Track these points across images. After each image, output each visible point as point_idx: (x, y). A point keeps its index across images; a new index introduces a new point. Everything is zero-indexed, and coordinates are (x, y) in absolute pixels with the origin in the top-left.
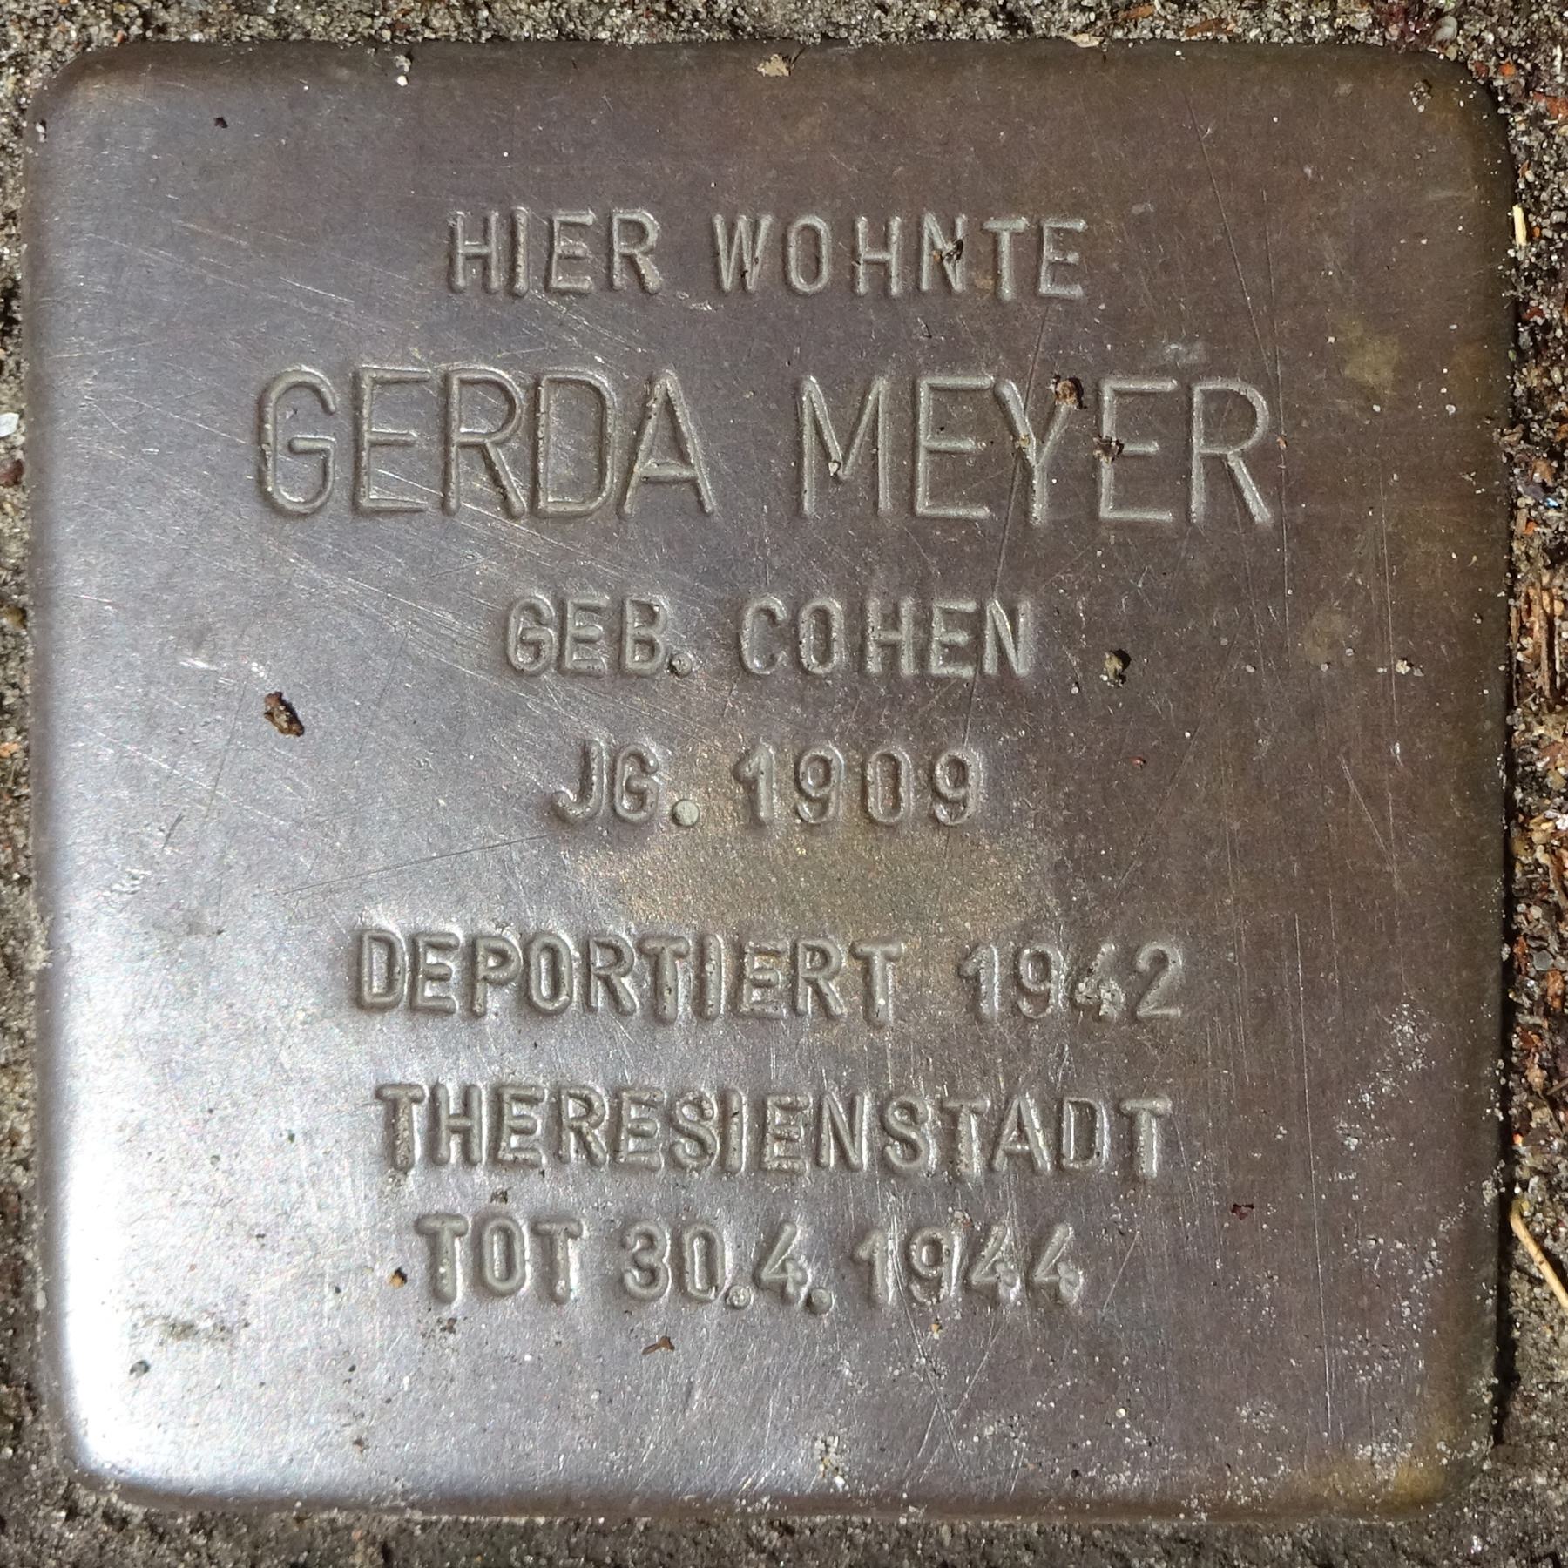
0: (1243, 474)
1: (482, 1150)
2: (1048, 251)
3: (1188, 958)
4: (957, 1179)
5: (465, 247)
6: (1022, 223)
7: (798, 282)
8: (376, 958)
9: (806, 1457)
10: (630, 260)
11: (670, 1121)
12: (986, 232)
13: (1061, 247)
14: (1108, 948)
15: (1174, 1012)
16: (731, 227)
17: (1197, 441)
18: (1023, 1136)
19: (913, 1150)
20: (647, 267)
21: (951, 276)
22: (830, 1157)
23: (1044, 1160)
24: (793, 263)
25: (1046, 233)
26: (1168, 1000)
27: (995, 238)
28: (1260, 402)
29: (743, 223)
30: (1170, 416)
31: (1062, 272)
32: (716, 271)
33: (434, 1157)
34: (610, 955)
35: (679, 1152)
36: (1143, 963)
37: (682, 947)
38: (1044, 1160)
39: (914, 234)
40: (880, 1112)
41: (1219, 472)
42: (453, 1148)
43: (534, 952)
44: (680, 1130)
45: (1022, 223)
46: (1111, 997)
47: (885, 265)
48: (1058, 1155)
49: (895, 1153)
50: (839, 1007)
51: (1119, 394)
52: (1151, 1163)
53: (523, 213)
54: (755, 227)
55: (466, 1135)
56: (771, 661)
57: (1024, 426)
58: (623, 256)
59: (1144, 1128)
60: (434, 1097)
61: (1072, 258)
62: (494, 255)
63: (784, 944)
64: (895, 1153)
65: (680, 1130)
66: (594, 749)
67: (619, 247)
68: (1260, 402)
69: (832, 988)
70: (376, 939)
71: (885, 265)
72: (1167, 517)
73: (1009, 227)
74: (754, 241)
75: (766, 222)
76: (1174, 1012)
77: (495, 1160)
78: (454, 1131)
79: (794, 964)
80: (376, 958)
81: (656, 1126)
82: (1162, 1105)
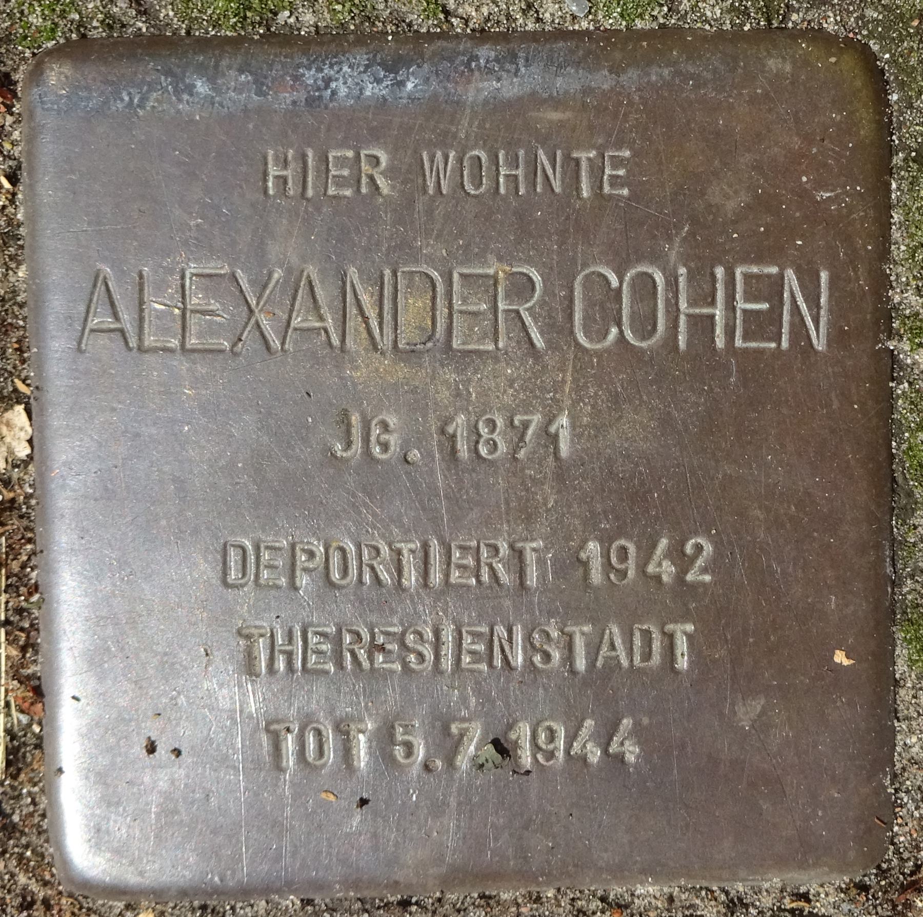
4: (573, 672)
5: (273, 171)
6: (592, 154)
8: (234, 557)
10: (371, 178)
12: (573, 159)
13: (614, 167)
14: (664, 543)
15: (707, 578)
18: (613, 647)
19: (547, 657)
20: (381, 181)
22: (498, 662)
24: (466, 178)
25: (331, 159)
26: (704, 570)
27: (577, 162)
29: (439, 154)
34: (374, 554)
36: (689, 549)
38: (625, 663)
39: (532, 164)
40: (528, 638)
42: (281, 665)
43: (331, 551)
45: (592, 154)
46: (668, 570)
47: (516, 176)
49: (537, 659)
50: (385, 576)
51: (334, 157)
52: (683, 663)
55: (289, 655)
58: (367, 175)
59: (679, 642)
60: (272, 636)
61: (621, 172)
62: (290, 177)
63: (474, 543)
64: (537, 659)
67: (365, 167)
69: (380, 568)
71: (516, 176)
73: (585, 156)
74: (446, 164)
75: (452, 154)
76: (707, 578)
78: (281, 652)
79: (293, 556)
80: (234, 557)
81: (394, 647)
82: (690, 628)
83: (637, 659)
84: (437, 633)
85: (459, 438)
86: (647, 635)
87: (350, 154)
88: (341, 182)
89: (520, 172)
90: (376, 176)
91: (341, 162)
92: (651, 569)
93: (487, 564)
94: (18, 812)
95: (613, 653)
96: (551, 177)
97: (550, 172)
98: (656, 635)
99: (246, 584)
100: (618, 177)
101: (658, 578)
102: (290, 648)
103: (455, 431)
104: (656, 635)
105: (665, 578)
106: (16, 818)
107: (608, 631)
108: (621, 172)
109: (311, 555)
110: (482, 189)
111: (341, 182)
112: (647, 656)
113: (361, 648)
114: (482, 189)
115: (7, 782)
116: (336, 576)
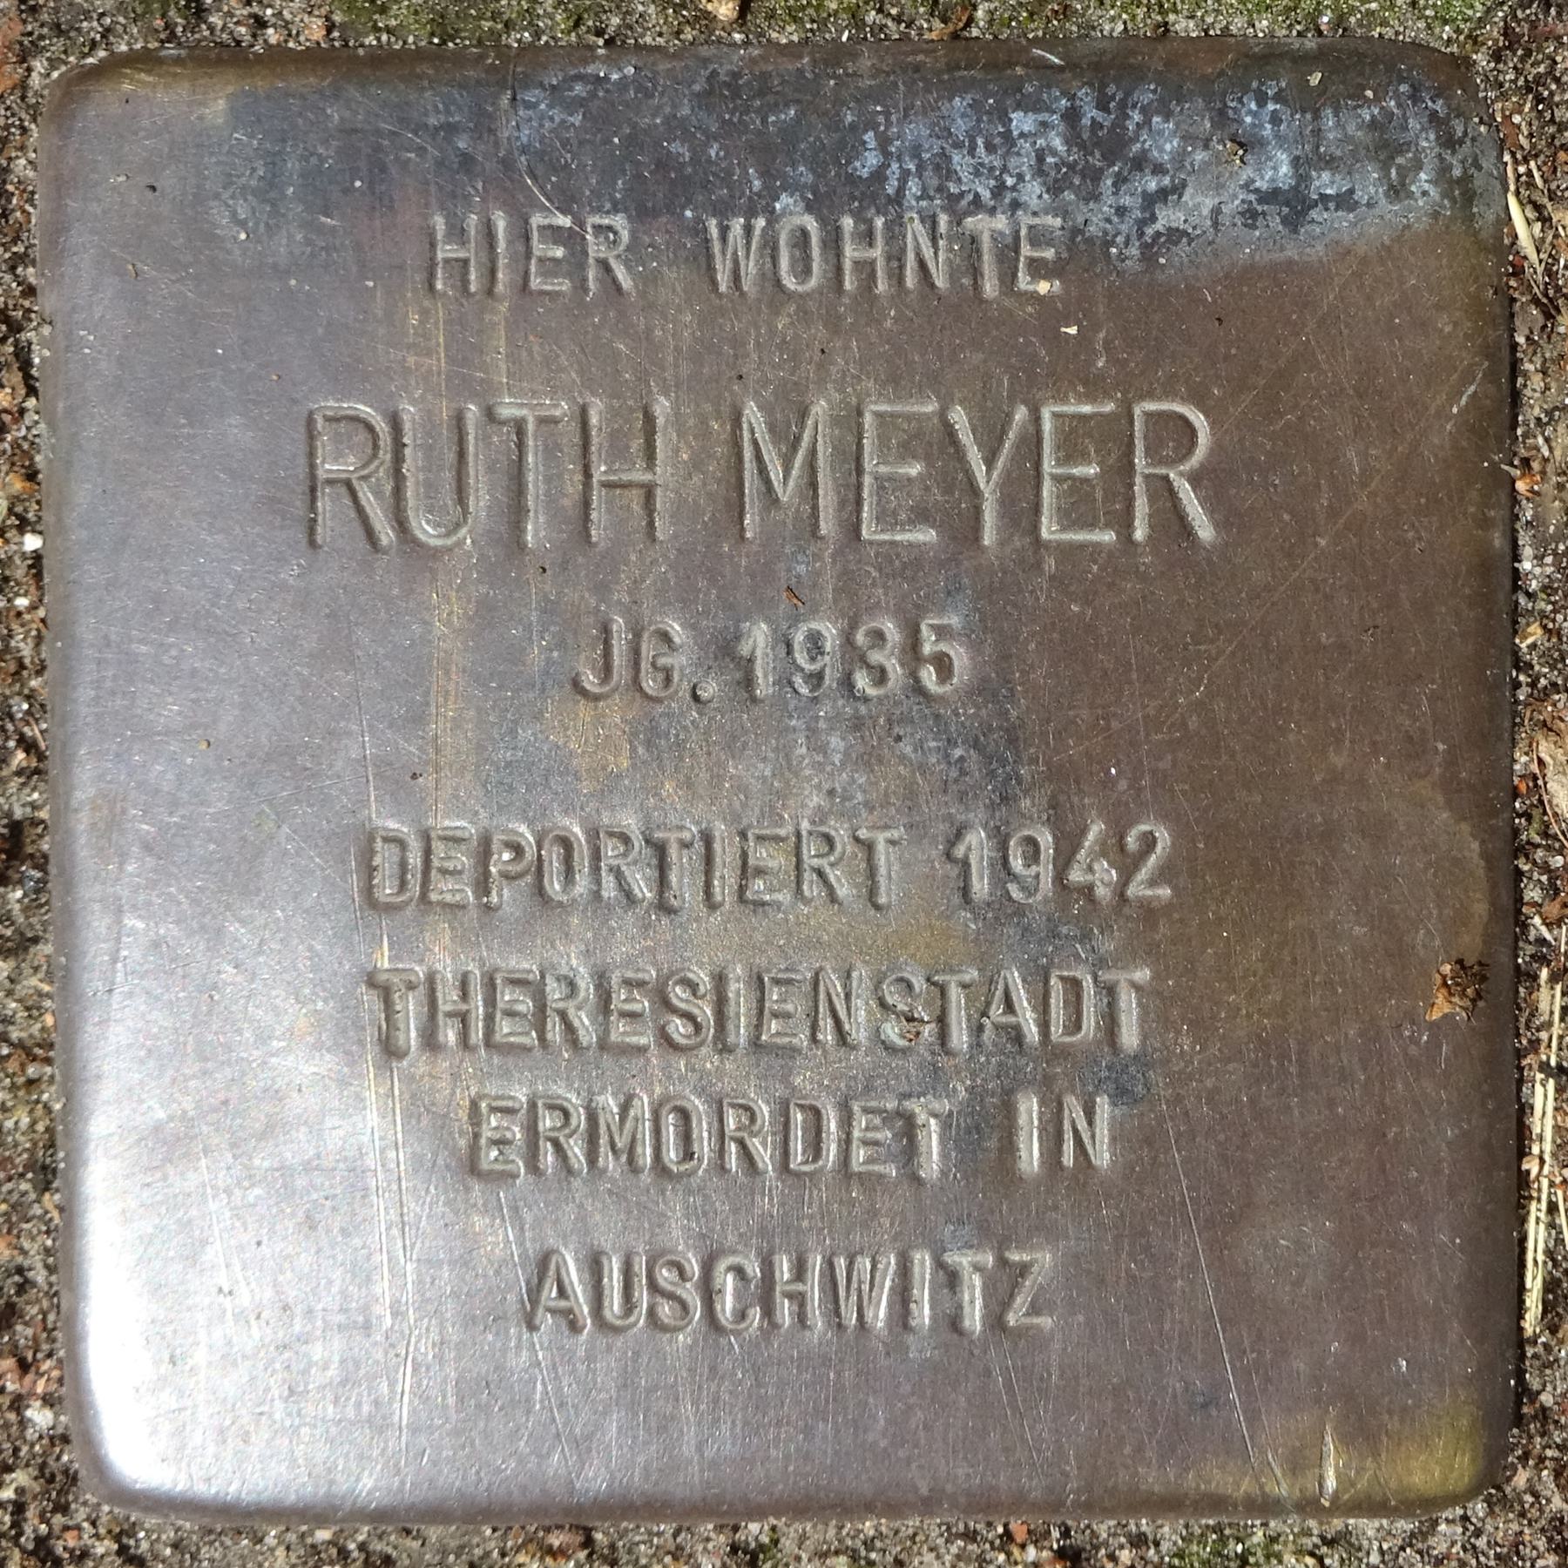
0: (1186, 492)
1: (477, 1034)
2: (1026, 250)
3: (1176, 838)
7: (790, 282)
8: (385, 858)
9: (706, 1446)
10: (604, 265)
11: (666, 1004)
13: (1035, 242)
16: (724, 231)
17: (1139, 461)
18: (1010, 1007)
21: (933, 270)
23: (1032, 1032)
26: (1152, 883)
28: (1198, 419)
29: (737, 224)
30: (1113, 439)
31: (1038, 269)
32: (711, 269)
33: (430, 1041)
35: (671, 1029)
36: (1131, 841)
37: (686, 836)
38: (1032, 1032)
41: (1163, 491)
42: (450, 1036)
44: (674, 1010)
46: (1104, 875)
48: (1044, 1026)
52: (1130, 1037)
53: (501, 224)
54: (748, 230)
55: (464, 1018)
56: (741, 1315)
57: (974, 456)
65: (674, 1010)
66: (615, 628)
68: (1198, 419)
70: (386, 840)
71: (873, 263)
72: (1108, 537)
74: (748, 244)
76: (1165, 892)
77: (489, 1042)
82: (1143, 975)
83: (1056, 1031)
84: (720, 980)
85: (759, 662)
86: (1074, 985)
87: (565, 221)
88: (550, 267)
89: (877, 253)
90: (613, 263)
91: (554, 234)
92: (1076, 876)
93: (814, 869)
94: (1549, 1388)
95: (1012, 1019)
96: (931, 265)
97: (928, 253)
98: (1088, 983)
99: (407, 903)
100: (1042, 260)
101: (1088, 891)
102: (464, 1007)
103: (753, 652)
104: (1088, 983)
105: (1101, 892)
106: (1546, 1399)
107: (1001, 982)
108: (1049, 254)
109: (518, 850)
110: (813, 282)
111: (550, 267)
112: (1075, 1025)
113: (579, 1008)
114: (813, 282)
115: (1543, 1339)
116: (555, 886)
